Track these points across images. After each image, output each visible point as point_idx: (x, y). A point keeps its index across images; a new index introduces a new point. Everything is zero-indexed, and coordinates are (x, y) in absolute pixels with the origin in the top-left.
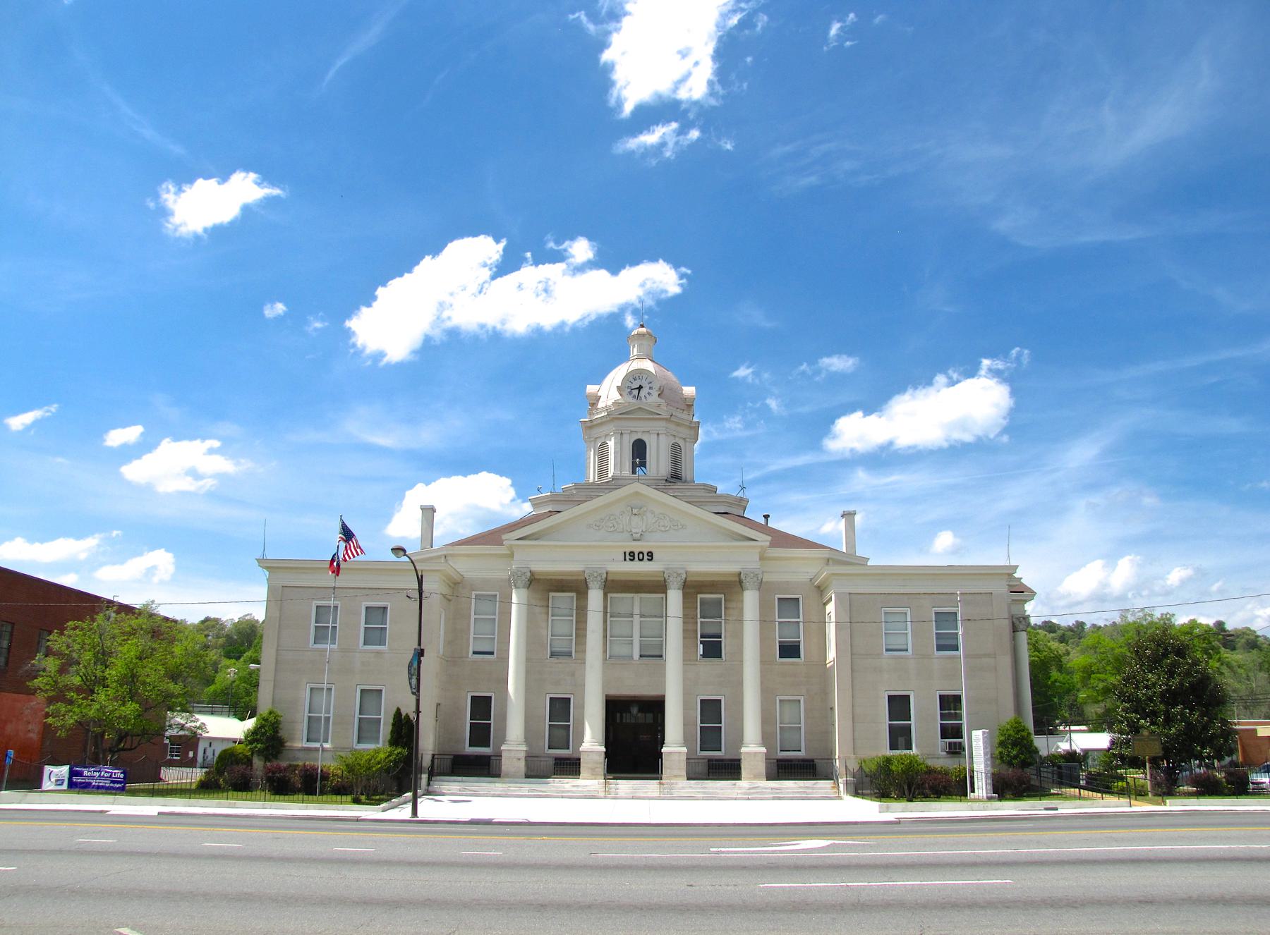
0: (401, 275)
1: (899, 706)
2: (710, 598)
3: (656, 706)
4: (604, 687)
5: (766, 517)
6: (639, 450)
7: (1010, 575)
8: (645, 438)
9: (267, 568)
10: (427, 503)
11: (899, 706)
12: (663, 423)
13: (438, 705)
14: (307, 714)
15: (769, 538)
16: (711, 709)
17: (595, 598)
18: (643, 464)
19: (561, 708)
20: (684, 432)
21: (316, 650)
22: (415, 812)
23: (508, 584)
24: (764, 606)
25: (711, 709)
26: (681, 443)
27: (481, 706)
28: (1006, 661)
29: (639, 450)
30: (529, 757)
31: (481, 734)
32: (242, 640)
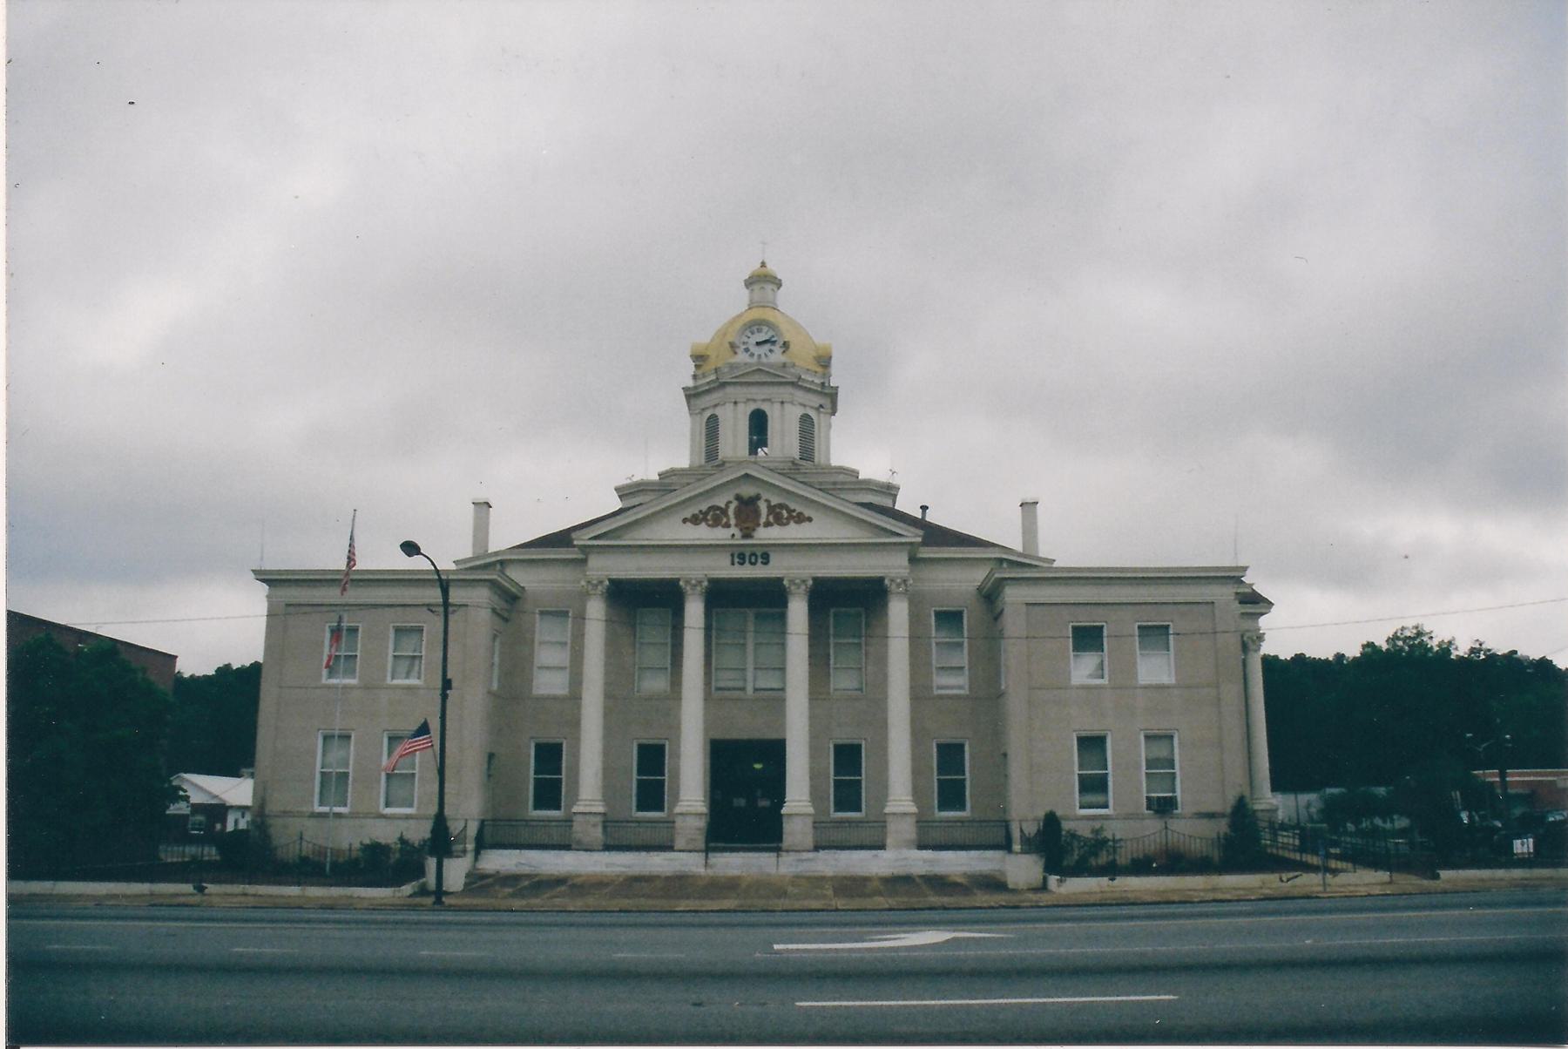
0: (1299, 659)
1: (1092, 745)
2: (848, 605)
3: (774, 751)
4: (706, 730)
5: (924, 508)
6: (759, 423)
7: (1238, 580)
8: (765, 407)
9: (263, 581)
10: (481, 498)
11: (1092, 745)
12: (790, 389)
13: (491, 756)
14: (318, 769)
15: (921, 532)
16: (848, 757)
17: (694, 611)
18: (764, 443)
19: (653, 759)
20: (816, 400)
21: (329, 687)
22: (340, 620)
23: (584, 596)
24: (915, 619)
25: (848, 757)
26: (813, 414)
27: (549, 756)
28: (1231, 692)
29: (759, 423)
30: (607, 822)
31: (549, 794)
32: (236, 690)
